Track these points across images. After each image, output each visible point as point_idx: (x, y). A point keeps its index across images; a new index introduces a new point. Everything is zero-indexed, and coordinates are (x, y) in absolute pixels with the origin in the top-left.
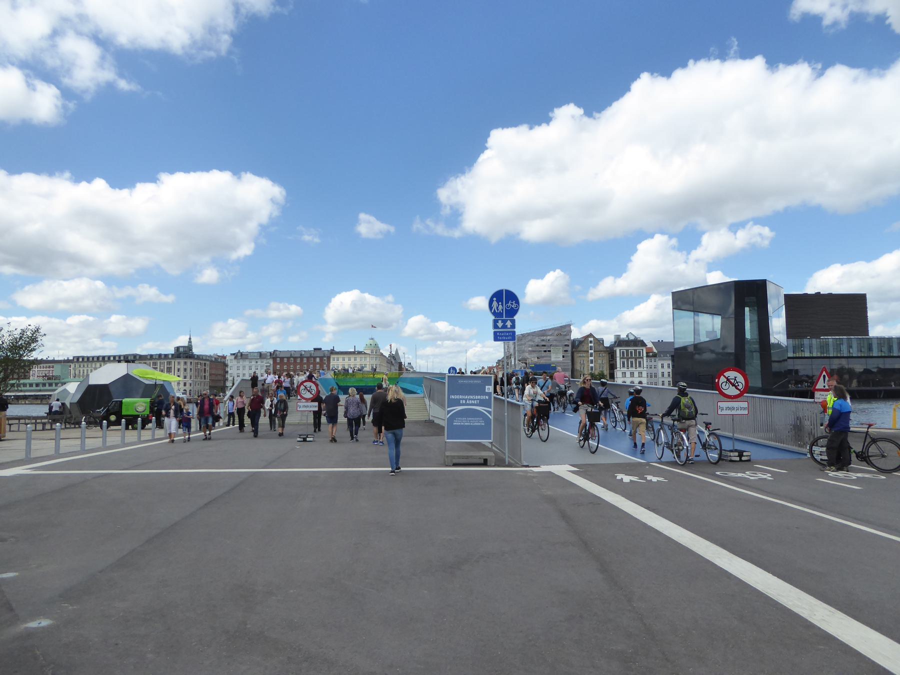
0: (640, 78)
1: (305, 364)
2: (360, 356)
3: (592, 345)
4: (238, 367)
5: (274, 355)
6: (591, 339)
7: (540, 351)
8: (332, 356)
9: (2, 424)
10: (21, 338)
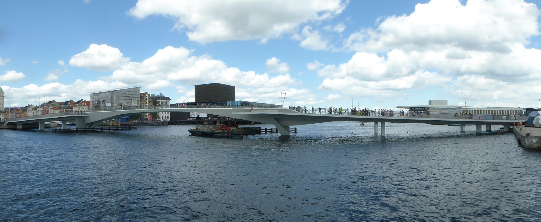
7: (128, 100)
10: (258, 149)
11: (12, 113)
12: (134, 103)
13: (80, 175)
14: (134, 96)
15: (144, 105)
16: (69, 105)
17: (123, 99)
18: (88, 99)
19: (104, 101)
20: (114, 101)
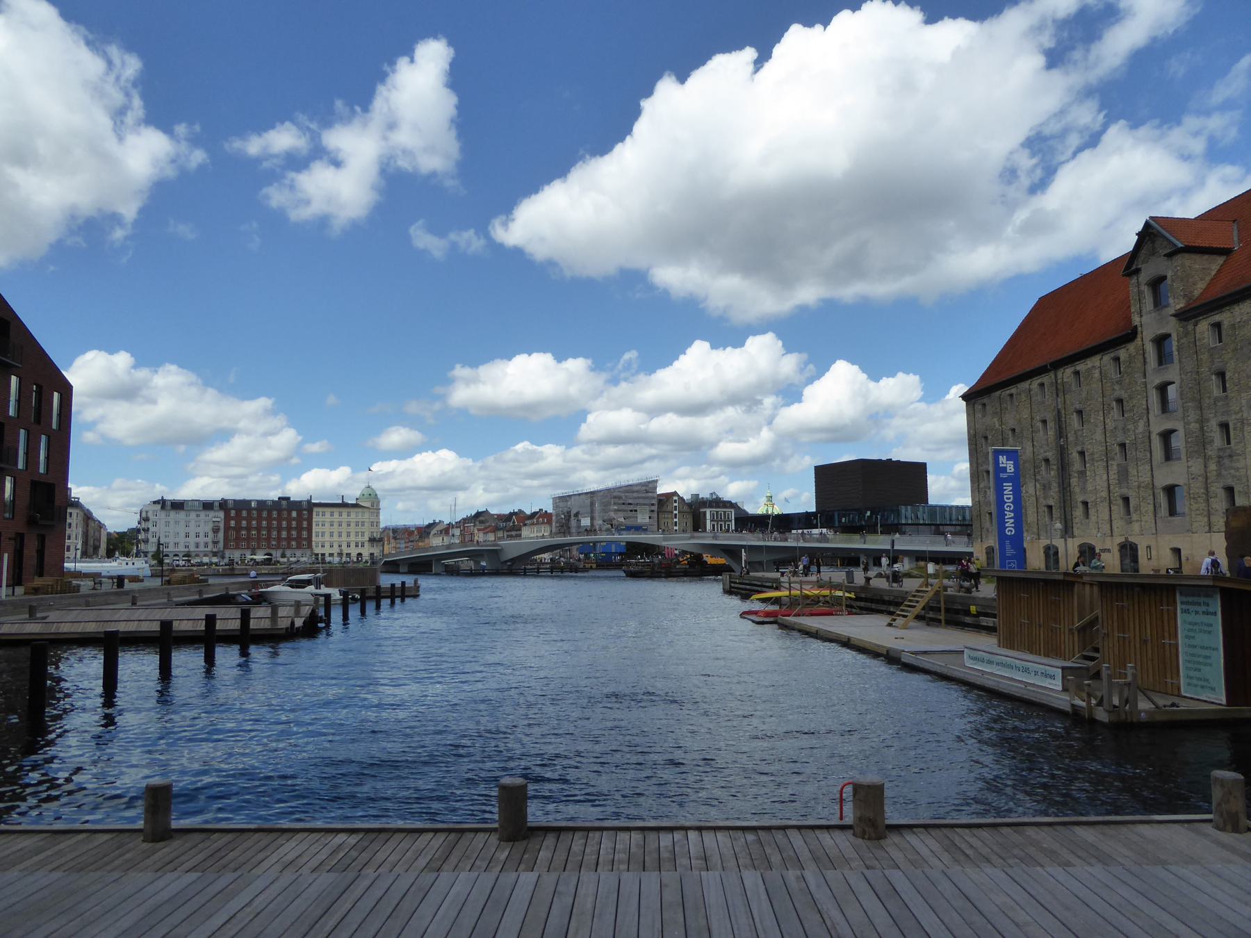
0: (530, 355)
1: (275, 519)
2: (356, 510)
3: (676, 504)
4: (166, 522)
5: (224, 504)
8: (315, 510)
9: (1196, 599)
11: (398, 541)
12: (643, 518)
13: (389, 693)
14: (641, 501)
15: (669, 521)
16: (514, 522)
17: (616, 510)
18: (550, 509)
19: (577, 515)
20: (596, 515)
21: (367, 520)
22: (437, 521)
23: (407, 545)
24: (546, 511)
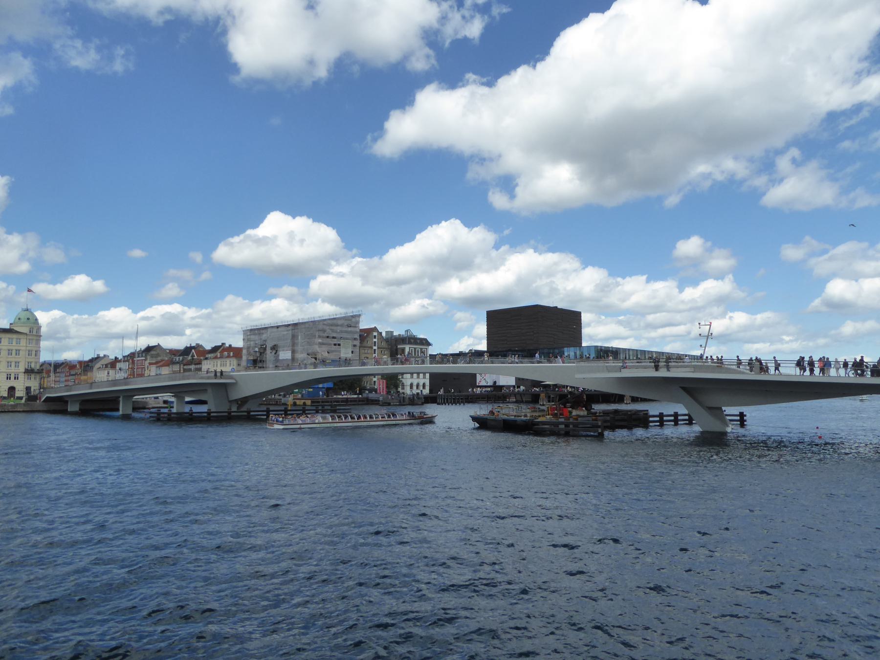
0: (294, 218)
6: (375, 334)
7: (330, 344)
11: (58, 375)
12: (346, 352)
16: (193, 356)
18: (238, 342)
20: (299, 348)
21: (24, 348)
22: (102, 355)
23: (67, 378)
24: (230, 346)
